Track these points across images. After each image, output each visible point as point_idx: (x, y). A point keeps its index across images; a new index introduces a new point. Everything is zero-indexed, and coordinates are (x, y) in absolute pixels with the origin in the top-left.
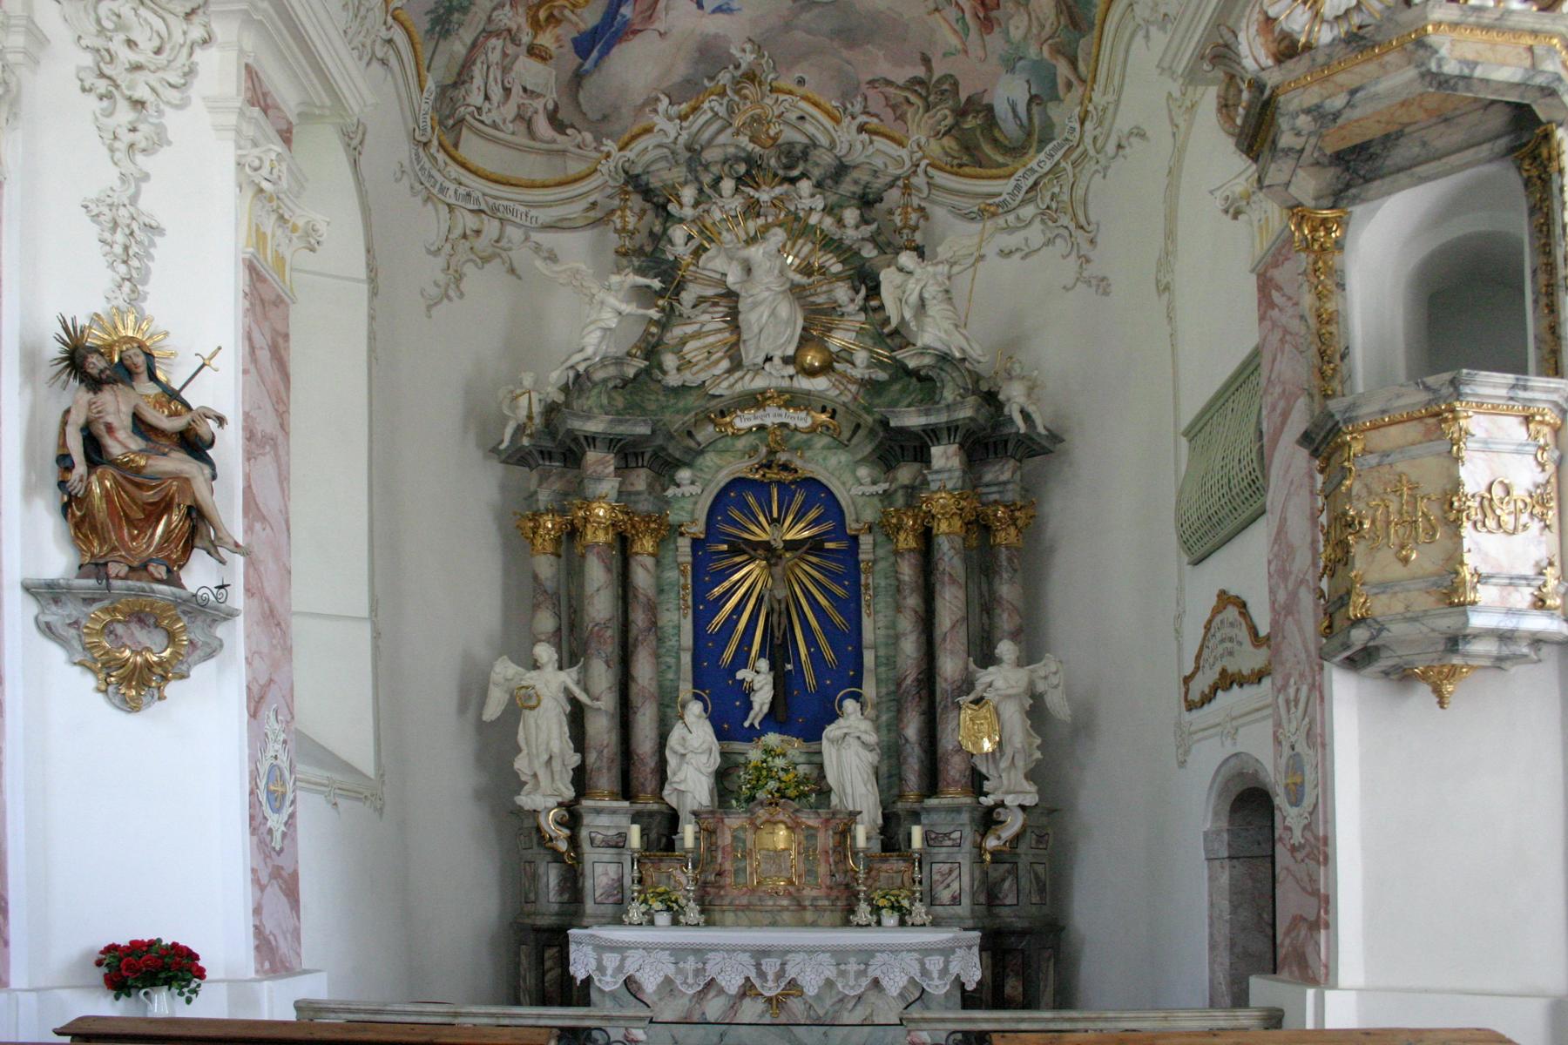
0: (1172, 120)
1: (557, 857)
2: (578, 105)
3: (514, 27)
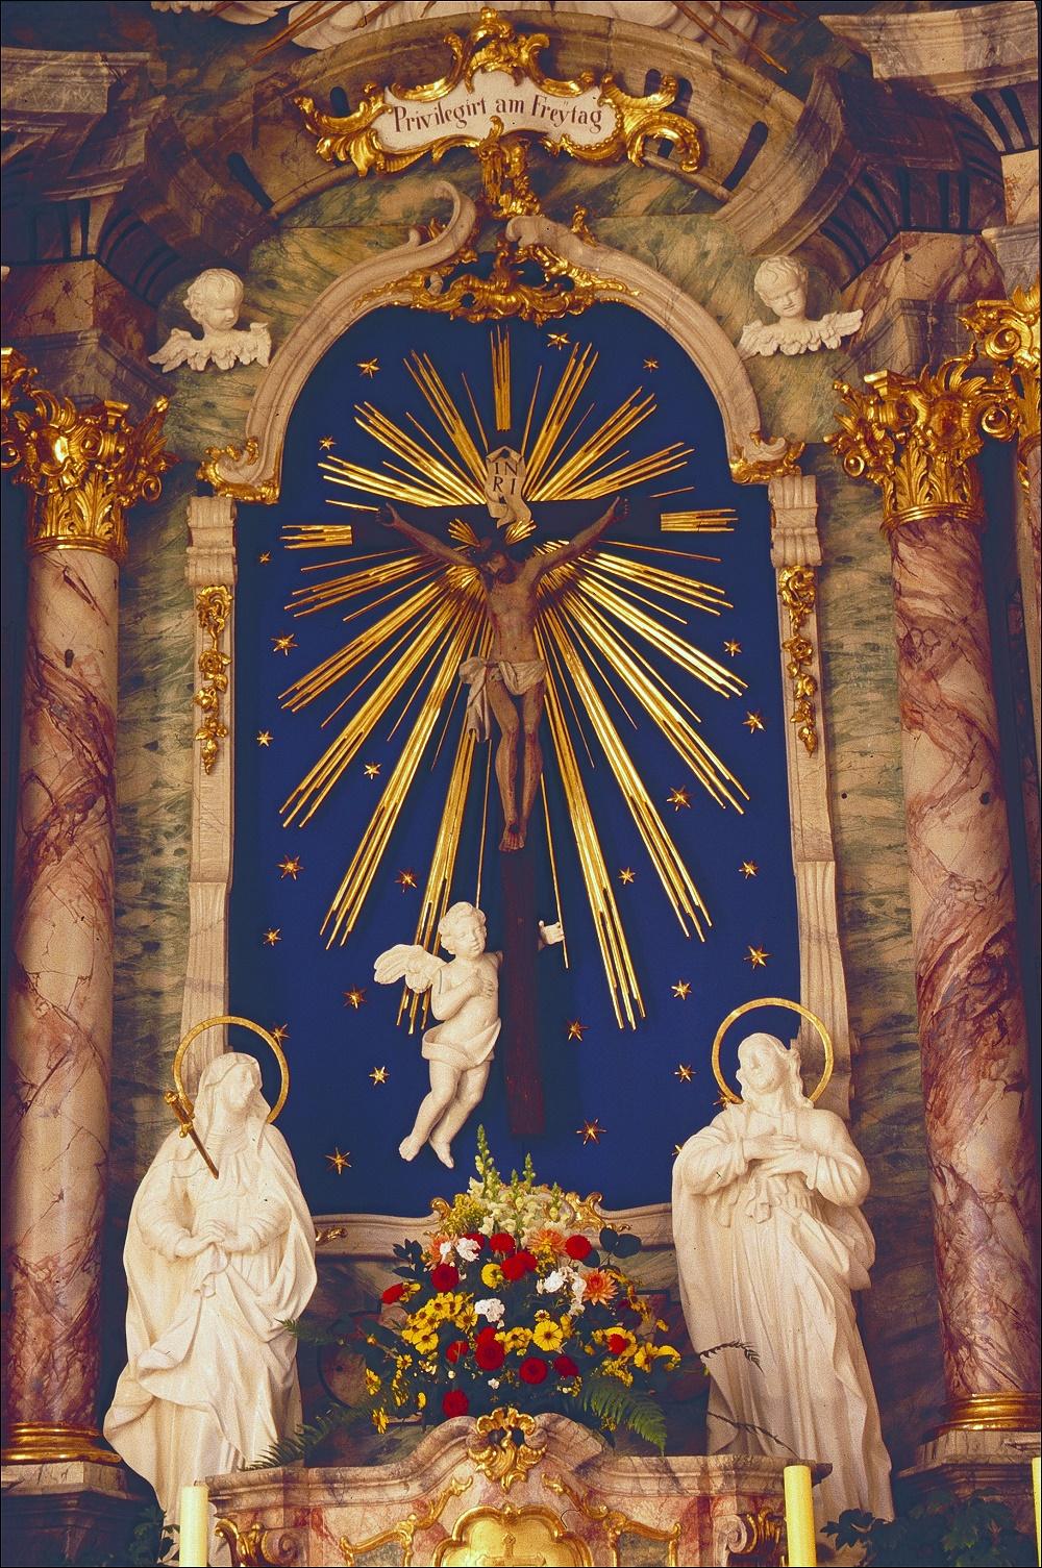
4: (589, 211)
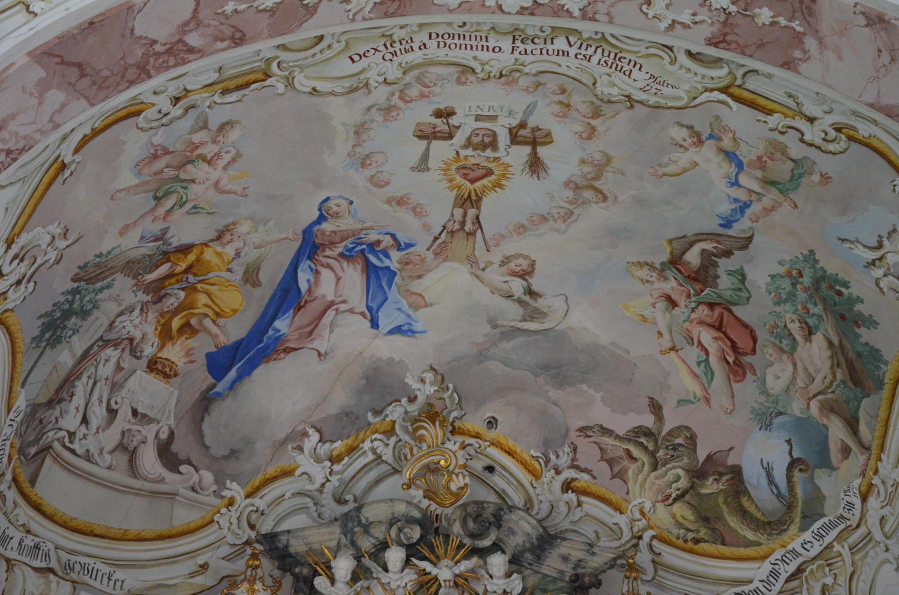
3: (138, 335)
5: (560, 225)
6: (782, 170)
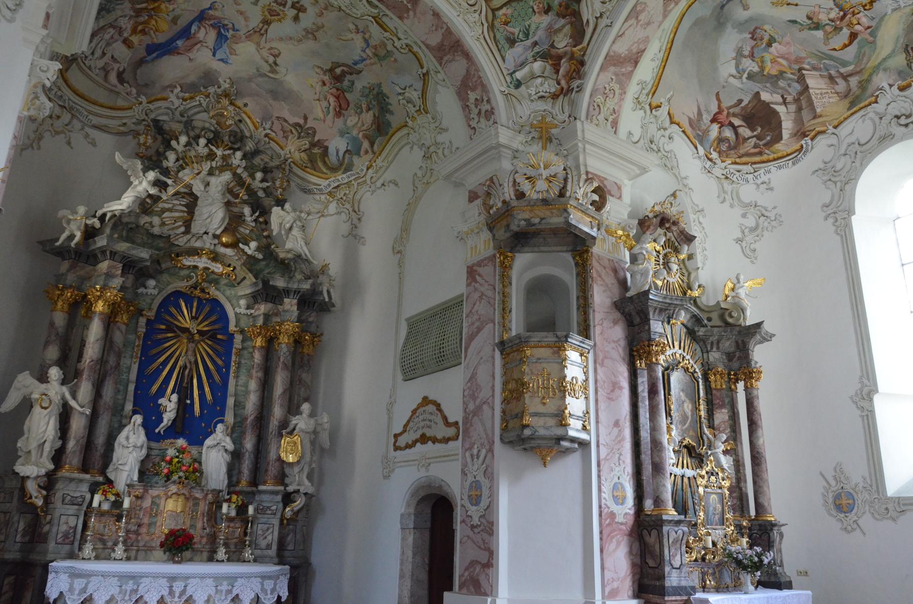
0: (414, 185)
1: (27, 507)
2: (136, 74)
3: (124, 27)
4: (216, 282)
5: (296, 43)
6: (382, 52)
